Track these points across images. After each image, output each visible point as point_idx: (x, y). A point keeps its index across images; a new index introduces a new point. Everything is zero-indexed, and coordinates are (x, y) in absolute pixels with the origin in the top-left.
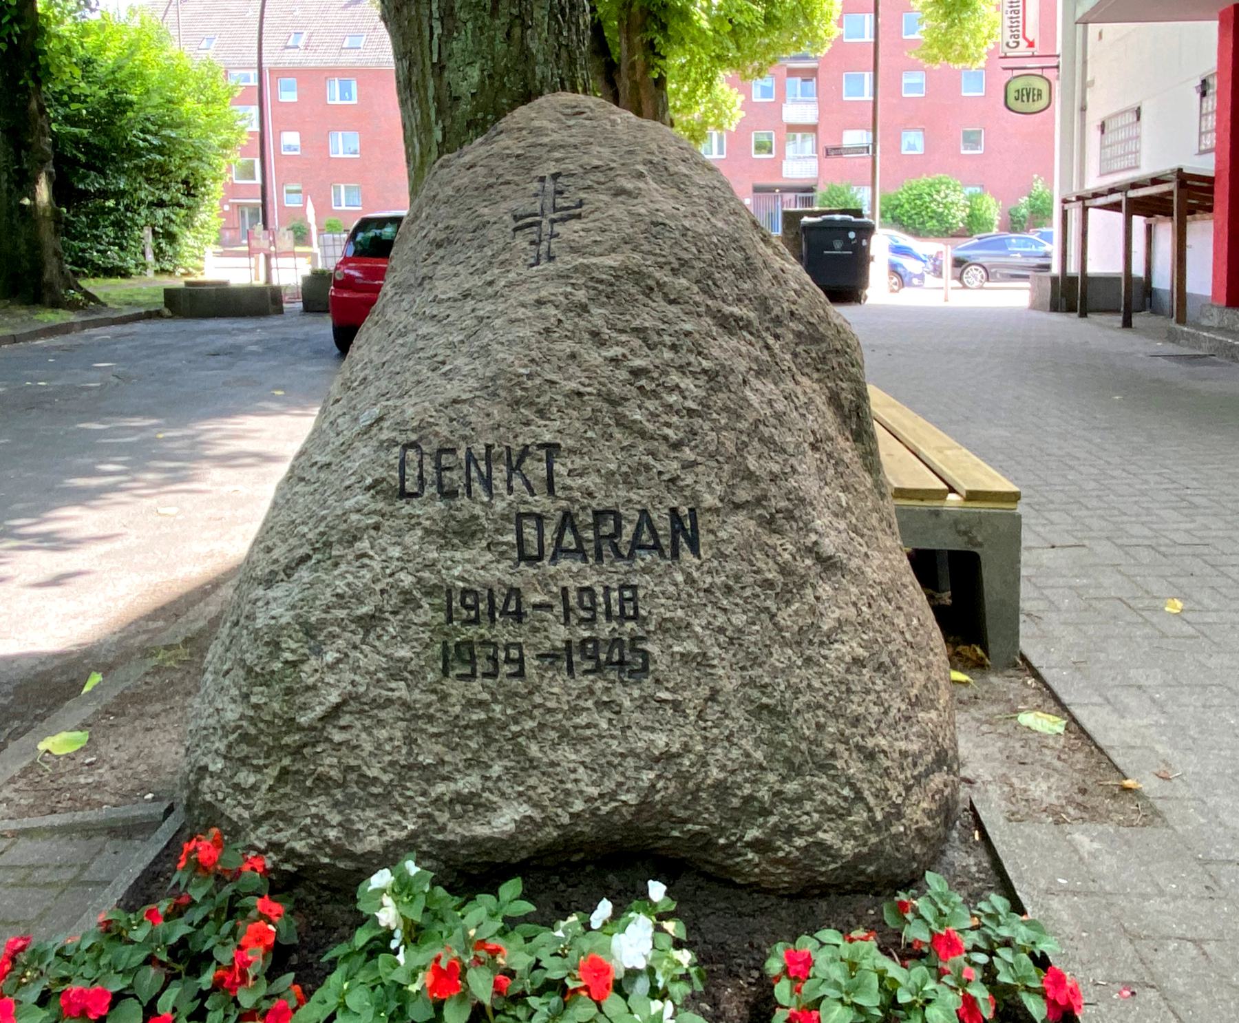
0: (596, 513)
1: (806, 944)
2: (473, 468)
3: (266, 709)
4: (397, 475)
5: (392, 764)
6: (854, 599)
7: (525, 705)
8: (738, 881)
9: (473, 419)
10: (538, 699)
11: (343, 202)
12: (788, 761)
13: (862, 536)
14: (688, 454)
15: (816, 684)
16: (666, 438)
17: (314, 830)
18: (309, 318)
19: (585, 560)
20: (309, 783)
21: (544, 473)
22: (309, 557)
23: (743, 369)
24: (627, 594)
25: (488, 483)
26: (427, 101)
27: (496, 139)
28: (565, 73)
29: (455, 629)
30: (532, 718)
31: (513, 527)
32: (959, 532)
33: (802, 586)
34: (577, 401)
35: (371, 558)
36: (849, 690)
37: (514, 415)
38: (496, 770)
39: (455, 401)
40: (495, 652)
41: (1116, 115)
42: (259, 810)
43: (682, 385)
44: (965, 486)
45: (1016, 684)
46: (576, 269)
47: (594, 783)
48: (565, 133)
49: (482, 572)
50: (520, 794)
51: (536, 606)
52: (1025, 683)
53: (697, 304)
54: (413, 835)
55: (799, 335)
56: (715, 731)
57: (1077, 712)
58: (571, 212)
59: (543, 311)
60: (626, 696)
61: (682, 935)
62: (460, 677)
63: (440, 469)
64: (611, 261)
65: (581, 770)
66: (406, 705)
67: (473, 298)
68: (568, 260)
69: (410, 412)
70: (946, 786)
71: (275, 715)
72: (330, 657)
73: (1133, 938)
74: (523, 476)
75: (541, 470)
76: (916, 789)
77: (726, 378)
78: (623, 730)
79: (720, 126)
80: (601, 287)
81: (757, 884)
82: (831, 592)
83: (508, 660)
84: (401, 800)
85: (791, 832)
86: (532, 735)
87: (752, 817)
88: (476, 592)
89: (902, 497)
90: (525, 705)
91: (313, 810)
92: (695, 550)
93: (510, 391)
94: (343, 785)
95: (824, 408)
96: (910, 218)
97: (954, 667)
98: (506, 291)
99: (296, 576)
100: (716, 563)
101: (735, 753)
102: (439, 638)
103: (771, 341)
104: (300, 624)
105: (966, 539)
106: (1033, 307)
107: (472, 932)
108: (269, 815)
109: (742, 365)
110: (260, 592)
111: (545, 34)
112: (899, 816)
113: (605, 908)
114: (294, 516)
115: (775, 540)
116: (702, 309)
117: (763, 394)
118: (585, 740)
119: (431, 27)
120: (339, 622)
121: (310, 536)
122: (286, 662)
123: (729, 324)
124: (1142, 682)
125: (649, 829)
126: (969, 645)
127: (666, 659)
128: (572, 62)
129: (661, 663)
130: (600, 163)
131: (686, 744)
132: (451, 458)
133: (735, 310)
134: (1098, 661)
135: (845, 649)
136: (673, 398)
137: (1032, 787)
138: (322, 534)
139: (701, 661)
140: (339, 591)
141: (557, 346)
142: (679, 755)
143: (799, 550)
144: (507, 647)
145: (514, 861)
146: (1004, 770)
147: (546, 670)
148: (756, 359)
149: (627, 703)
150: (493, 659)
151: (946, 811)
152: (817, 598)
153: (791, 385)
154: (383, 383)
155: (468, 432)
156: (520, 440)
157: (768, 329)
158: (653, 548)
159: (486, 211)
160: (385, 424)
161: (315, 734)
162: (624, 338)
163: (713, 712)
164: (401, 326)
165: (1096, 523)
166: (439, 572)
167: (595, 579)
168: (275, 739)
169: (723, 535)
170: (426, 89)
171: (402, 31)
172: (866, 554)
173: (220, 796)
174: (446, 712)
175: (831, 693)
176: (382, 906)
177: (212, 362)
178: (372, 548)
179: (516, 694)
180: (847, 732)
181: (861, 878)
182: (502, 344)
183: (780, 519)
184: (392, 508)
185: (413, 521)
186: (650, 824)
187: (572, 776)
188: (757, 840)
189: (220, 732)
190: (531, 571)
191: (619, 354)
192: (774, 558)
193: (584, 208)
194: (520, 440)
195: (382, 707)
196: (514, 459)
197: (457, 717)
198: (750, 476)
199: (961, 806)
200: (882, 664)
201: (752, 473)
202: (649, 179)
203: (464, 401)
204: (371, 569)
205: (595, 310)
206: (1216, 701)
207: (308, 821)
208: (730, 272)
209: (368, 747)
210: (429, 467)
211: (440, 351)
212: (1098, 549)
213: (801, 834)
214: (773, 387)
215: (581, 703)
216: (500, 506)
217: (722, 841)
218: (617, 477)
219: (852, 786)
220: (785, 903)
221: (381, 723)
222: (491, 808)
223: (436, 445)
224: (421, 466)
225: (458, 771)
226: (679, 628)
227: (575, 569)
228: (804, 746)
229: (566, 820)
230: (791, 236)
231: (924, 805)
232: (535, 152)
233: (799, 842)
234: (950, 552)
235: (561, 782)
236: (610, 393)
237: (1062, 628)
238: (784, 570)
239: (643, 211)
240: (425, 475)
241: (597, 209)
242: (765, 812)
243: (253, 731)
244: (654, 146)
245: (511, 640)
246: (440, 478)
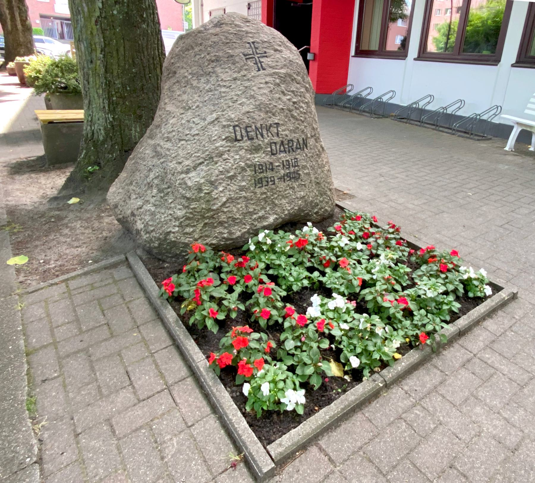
3: (198, 208)
4: (234, 135)
5: (242, 213)
9: (255, 117)
10: (278, 189)
16: (301, 120)
19: (286, 153)
21: (276, 131)
22: (203, 162)
25: (262, 136)
30: (276, 194)
34: (282, 111)
38: (268, 209)
39: (248, 112)
41: (215, 10)
46: (274, 73)
47: (289, 206)
51: (277, 166)
60: (295, 185)
62: (259, 187)
63: (247, 132)
64: (283, 71)
66: (245, 197)
71: (203, 209)
72: (221, 189)
83: (271, 181)
85: (320, 209)
86: (276, 198)
91: (218, 231)
93: (265, 108)
99: (198, 169)
101: (314, 194)
108: (201, 237)
110: (184, 176)
114: (189, 151)
118: (287, 197)
120: (222, 179)
121: (202, 156)
122: (206, 193)
138: (208, 155)
139: (308, 174)
141: (274, 95)
144: (270, 178)
149: (296, 187)
150: (267, 182)
155: (254, 121)
156: (269, 122)
159: (230, 51)
161: (218, 211)
162: (290, 93)
168: (201, 216)
179: (273, 189)
189: (174, 220)
194: (269, 122)
195: (238, 199)
203: (251, 112)
204: (230, 163)
216: (266, 141)
221: (238, 203)
222: (267, 218)
223: (244, 125)
224: (241, 131)
229: (283, 216)
233: (323, 210)
243: (191, 216)
246: (248, 135)
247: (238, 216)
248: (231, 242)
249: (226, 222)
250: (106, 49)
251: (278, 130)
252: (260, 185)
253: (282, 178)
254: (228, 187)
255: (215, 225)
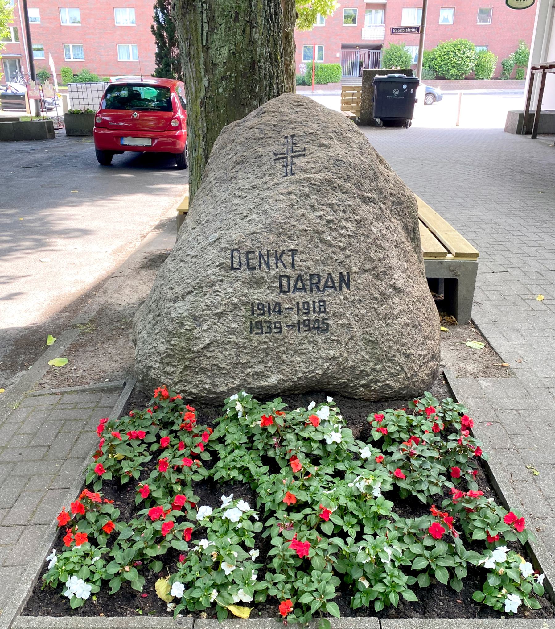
0: (310, 275)
1: (381, 413)
2: (262, 259)
3: (178, 346)
4: (230, 261)
5: (230, 363)
6: (407, 302)
7: (282, 342)
8: (356, 397)
9: (262, 240)
10: (286, 340)
11: (72, 57)
12: (378, 359)
13: (412, 279)
14: (348, 252)
15: (390, 333)
16: (339, 247)
17: (199, 385)
18: (73, 141)
19: (306, 292)
20: (197, 370)
21: (291, 261)
23: (371, 218)
24: (322, 304)
26: (199, 65)
27: (262, 115)
28: (271, 50)
29: (255, 317)
30: (284, 347)
31: (278, 280)
32: (450, 270)
33: (387, 299)
34: (304, 233)
35: (220, 292)
36: (402, 334)
37: (279, 239)
38: (270, 364)
39: (253, 233)
40: (271, 325)
42: (176, 379)
43: (347, 226)
44: (454, 251)
45: (467, 331)
46: (304, 179)
47: (306, 368)
48: (296, 115)
49: (266, 297)
50: (279, 372)
51: (286, 309)
52: (471, 331)
53: (354, 194)
54: (239, 386)
55: (393, 202)
56: (352, 349)
57: (490, 340)
58: (300, 153)
59: (290, 197)
60: (319, 339)
61: (339, 411)
62: (257, 333)
63: (248, 259)
64: (318, 176)
65: (302, 363)
66: (235, 343)
67: (258, 189)
68: (300, 176)
69: (234, 237)
70: (434, 365)
71: (183, 348)
72: (205, 328)
73: (495, 410)
74: (282, 262)
75: (290, 259)
76: (423, 367)
77: (364, 222)
78: (318, 350)
79: (324, 13)
80: (315, 187)
81: (363, 398)
82: (398, 300)
83: (275, 327)
84: (234, 375)
85: (376, 381)
87: (363, 377)
88: (263, 304)
89: (427, 256)
90: (282, 342)
91: (199, 379)
92: (348, 287)
94: (211, 370)
95: (401, 231)
96: (440, 67)
97: (442, 325)
98: (273, 187)
99: (187, 298)
100: (356, 292)
102: (248, 320)
103: (382, 206)
104: (191, 316)
105: (453, 273)
106: (507, 130)
107: (274, 409)
108: (181, 381)
109: (370, 217)
110: (171, 304)
111: (262, 30)
112: (416, 375)
113: (313, 404)
114: (183, 276)
115: (379, 283)
116: (356, 195)
117: (378, 228)
118: (303, 353)
119: (202, 27)
120: (208, 315)
121: (192, 284)
122: (187, 329)
123: (366, 201)
124: (519, 328)
125: (325, 382)
126: (449, 316)
127: (335, 326)
128: (275, 43)
129: (334, 327)
130: (312, 131)
131: (341, 354)
132: (253, 255)
133: (369, 195)
134: (503, 320)
135: (402, 320)
136: (343, 231)
137: (468, 367)
138: (198, 283)
140: (207, 304)
141: (297, 211)
142: (338, 358)
143: (388, 286)
144: (275, 323)
145: (275, 393)
146: (458, 362)
147: (290, 331)
148: (376, 214)
149: (320, 341)
150: (270, 328)
151: (434, 374)
152: (393, 303)
153: (389, 223)
154: (218, 223)
155: (259, 245)
156: (281, 248)
157: (381, 201)
158: (332, 287)
159: (260, 150)
160: (222, 241)
161: (199, 354)
162: (324, 208)
163: (351, 343)
164: (223, 198)
165: (515, 261)
166: (248, 297)
167: (309, 299)
168: (182, 356)
169: (359, 281)
170: (199, 59)
171: (185, 27)
172: (413, 286)
173: (159, 376)
174: (251, 346)
175: (395, 336)
176: (236, 404)
177: (28, 172)
178: (220, 288)
179: (278, 339)
180: (400, 348)
181: (401, 395)
182: (273, 210)
183: (381, 275)
184: (228, 274)
185: (237, 279)
186: (326, 380)
187: (298, 365)
188: (364, 384)
189: (156, 354)
190: (285, 296)
191: (322, 214)
192: (378, 289)
193: (306, 152)
194: (281, 248)
196: (279, 256)
197: (255, 347)
198: (371, 259)
199: (439, 373)
200: (415, 325)
201: (372, 258)
202: (334, 139)
203: (258, 233)
205: (312, 197)
206: (547, 335)
207: (197, 382)
208: (367, 180)
209: (221, 357)
210: (243, 258)
211: (245, 211)
212: (514, 273)
213: (380, 382)
214: (382, 224)
215: (303, 341)
216: (273, 273)
217: (352, 385)
218: (320, 261)
219: (400, 366)
220: (372, 404)
221: (226, 349)
222: (268, 376)
223: (246, 250)
224: (240, 258)
225: (256, 365)
226: (341, 315)
227: (302, 295)
228: (384, 354)
230: (367, 86)
231: (426, 372)
232: (283, 124)
233: (379, 384)
234: (445, 279)
235: (294, 367)
236: (318, 229)
237: (491, 307)
238: (381, 293)
239: (332, 155)
240: (242, 261)
241: (312, 153)
242: (368, 375)
243: (172, 353)
244: (336, 124)
245: (277, 320)
246: (248, 263)
247: (224, 366)
248: (215, 396)
249: (209, 370)
250: (208, 135)
251: (293, 259)
252: (260, 331)
253: (297, 326)
254: (214, 326)
255: (197, 370)
